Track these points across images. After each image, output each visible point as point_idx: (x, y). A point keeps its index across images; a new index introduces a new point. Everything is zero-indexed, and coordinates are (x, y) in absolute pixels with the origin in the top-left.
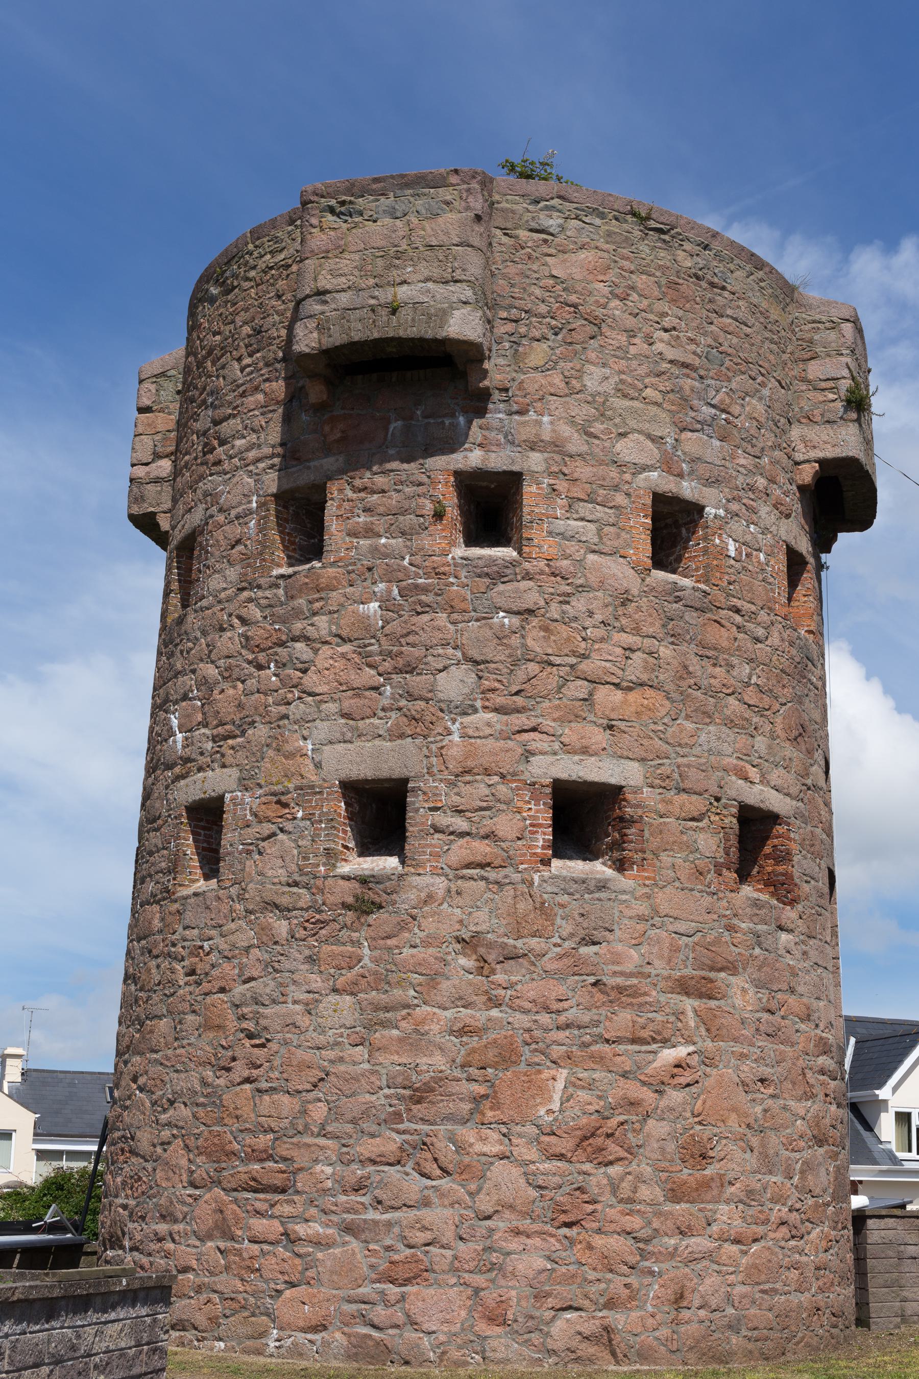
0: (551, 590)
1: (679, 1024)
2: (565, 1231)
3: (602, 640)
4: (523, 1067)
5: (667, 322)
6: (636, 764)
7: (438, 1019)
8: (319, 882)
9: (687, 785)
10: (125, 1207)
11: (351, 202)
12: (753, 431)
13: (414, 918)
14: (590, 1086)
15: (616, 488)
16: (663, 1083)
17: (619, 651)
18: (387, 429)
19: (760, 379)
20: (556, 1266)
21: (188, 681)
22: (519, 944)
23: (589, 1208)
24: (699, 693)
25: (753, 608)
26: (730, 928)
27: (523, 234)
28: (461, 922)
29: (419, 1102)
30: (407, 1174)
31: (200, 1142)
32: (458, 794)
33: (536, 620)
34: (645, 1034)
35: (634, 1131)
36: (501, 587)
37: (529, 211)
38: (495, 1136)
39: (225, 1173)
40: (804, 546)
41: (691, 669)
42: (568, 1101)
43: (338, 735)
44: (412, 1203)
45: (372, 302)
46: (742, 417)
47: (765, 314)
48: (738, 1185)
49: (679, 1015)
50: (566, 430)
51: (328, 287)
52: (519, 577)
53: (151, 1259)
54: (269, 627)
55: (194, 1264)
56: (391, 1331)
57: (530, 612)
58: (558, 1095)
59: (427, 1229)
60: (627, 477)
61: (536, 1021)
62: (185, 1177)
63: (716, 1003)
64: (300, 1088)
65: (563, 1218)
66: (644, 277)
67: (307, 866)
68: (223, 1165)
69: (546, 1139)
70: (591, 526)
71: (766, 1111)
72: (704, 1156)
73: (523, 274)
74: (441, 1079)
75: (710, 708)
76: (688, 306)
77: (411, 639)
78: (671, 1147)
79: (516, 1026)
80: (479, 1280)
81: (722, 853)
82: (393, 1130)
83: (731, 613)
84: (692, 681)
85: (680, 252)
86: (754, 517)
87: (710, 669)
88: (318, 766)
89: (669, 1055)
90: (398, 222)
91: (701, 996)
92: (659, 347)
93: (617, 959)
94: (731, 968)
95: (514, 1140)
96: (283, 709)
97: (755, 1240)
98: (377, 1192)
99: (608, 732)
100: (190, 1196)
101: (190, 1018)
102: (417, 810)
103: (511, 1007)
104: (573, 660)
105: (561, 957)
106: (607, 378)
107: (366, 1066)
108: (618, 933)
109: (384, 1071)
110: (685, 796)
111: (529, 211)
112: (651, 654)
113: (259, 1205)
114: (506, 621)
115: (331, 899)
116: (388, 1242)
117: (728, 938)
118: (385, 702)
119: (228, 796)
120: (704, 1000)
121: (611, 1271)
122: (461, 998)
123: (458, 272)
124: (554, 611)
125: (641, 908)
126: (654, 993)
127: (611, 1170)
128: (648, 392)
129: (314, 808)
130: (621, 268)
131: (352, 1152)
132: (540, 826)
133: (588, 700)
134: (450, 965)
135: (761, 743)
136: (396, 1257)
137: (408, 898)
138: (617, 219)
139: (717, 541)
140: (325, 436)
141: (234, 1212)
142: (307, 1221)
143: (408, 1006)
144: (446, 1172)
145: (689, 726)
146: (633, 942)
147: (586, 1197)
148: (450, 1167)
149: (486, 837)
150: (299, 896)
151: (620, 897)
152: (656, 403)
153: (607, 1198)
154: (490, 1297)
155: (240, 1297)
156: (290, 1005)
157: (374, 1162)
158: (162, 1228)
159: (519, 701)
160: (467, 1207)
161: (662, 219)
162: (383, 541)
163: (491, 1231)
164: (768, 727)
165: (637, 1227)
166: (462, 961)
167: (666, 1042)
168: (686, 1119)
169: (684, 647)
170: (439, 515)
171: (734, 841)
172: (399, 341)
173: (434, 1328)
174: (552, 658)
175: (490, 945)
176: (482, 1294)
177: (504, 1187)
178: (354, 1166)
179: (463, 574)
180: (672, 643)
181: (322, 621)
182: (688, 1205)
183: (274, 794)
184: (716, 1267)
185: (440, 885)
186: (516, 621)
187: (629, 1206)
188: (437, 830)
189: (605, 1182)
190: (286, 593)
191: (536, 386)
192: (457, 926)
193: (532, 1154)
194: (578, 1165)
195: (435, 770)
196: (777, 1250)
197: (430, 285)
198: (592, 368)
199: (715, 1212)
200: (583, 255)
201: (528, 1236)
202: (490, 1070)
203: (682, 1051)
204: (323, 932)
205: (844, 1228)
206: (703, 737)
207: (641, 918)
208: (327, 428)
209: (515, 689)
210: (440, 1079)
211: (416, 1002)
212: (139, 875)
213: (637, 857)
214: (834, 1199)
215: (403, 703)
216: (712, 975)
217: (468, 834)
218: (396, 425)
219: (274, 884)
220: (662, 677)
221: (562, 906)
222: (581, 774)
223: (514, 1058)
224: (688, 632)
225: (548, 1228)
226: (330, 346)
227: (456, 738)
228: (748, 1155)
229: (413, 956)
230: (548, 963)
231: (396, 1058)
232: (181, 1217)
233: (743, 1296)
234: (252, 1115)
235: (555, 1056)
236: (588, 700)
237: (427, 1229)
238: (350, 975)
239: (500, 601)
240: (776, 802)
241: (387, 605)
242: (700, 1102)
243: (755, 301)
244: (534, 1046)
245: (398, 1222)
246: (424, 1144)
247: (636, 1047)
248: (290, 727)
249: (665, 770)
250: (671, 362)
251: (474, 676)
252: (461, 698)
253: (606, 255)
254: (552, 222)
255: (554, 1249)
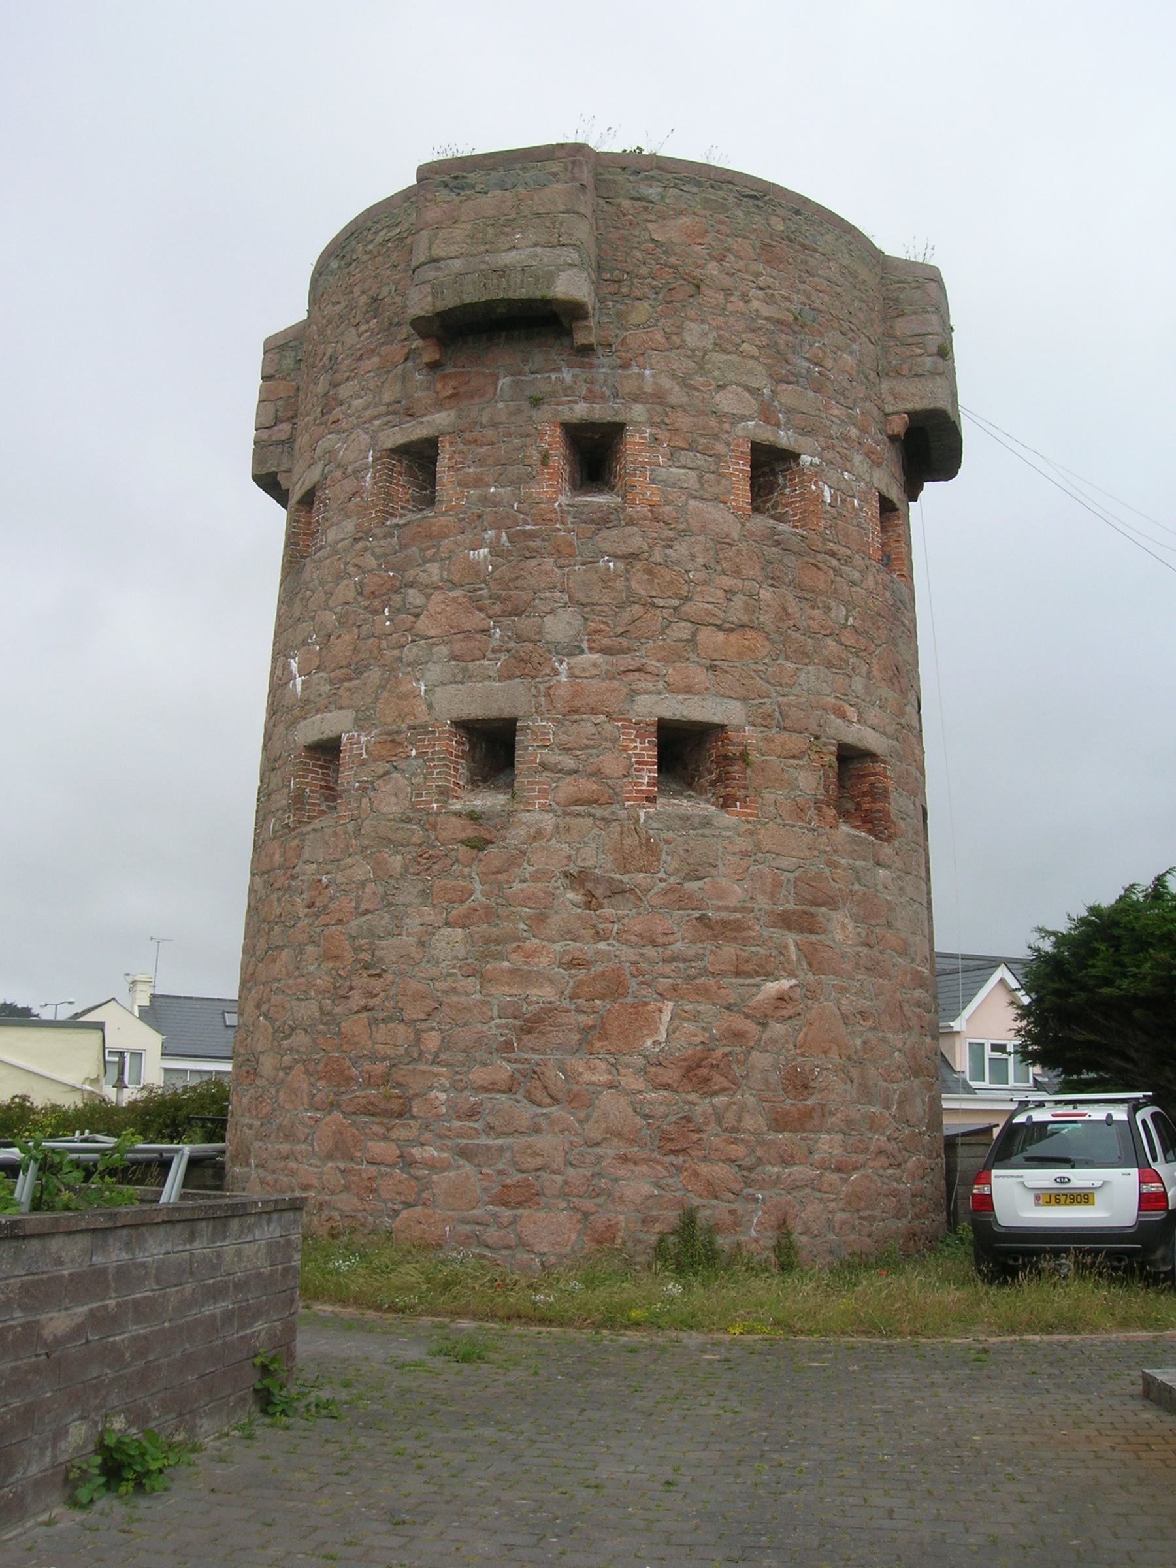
0: (655, 535)
1: (782, 958)
2: (671, 1158)
3: (705, 583)
4: (629, 1000)
5: (762, 281)
6: (738, 704)
7: (547, 954)
8: (431, 819)
9: (788, 723)
10: (250, 1127)
11: (464, 177)
12: (845, 384)
13: (524, 853)
14: (696, 1017)
15: (716, 437)
16: (766, 1016)
17: (720, 593)
18: (496, 386)
19: (851, 335)
20: (663, 1192)
21: (307, 626)
22: (625, 878)
23: (695, 1137)
24: (797, 635)
25: (849, 552)
26: (832, 864)
27: (626, 204)
28: (569, 857)
29: (529, 1032)
30: (518, 1102)
31: (320, 1067)
32: (565, 733)
33: (641, 564)
34: (748, 967)
35: (738, 1062)
36: (605, 533)
37: (629, 181)
38: (604, 1066)
39: (344, 1097)
40: (895, 494)
41: (790, 610)
42: (674, 1032)
43: (449, 676)
44: (523, 1129)
45: (483, 267)
46: (834, 371)
47: (854, 275)
48: (839, 1115)
49: (782, 949)
50: (666, 383)
51: (442, 254)
52: (623, 523)
53: (275, 1176)
54: (383, 573)
55: (315, 1182)
56: (504, 1252)
57: (634, 556)
58: (667, 1028)
59: (538, 1155)
60: (726, 426)
61: (642, 954)
62: (306, 1100)
63: (817, 937)
64: (415, 1017)
65: (670, 1146)
66: (739, 240)
67: (419, 803)
68: (343, 1089)
69: (653, 1069)
70: (693, 474)
71: (864, 1043)
72: (805, 1086)
73: (623, 238)
74: (551, 1010)
75: (809, 649)
76: (781, 266)
77: (519, 583)
78: (774, 1078)
79: (623, 959)
80: (588, 1204)
81: (822, 791)
82: (504, 1059)
83: (828, 557)
84: (791, 623)
85: (773, 218)
86: (848, 464)
87: (809, 611)
88: (430, 706)
89: (772, 988)
90: (507, 193)
91: (802, 930)
92: (755, 304)
93: (721, 894)
94: (831, 903)
95: (622, 1071)
96: (396, 652)
97: (855, 1168)
98: (490, 1119)
99: (710, 672)
100: (310, 1117)
101: (310, 948)
102: (526, 748)
103: (618, 941)
104: (676, 603)
105: (666, 892)
106: (706, 334)
107: (477, 996)
108: (722, 869)
109: (496, 1002)
110: (786, 734)
111: (629, 181)
112: (751, 596)
113: (376, 1128)
114: (611, 564)
115: (443, 835)
116: (500, 1166)
117: (828, 874)
118: (495, 643)
119: (344, 737)
120: (806, 935)
121: (716, 1198)
122: (569, 932)
123: (564, 237)
124: (657, 556)
125: (744, 844)
126: (757, 928)
127: (715, 1100)
128: (745, 346)
129: (427, 747)
130: (718, 231)
131: (465, 1079)
132: (646, 763)
133: (692, 641)
134: (558, 898)
135: (858, 684)
136: (508, 1181)
137: (516, 836)
138: (712, 187)
139: (814, 487)
140: (437, 393)
141: (353, 1135)
142: (423, 1145)
143: (518, 939)
144: (555, 1100)
145: (790, 666)
146: (737, 877)
147: (691, 1126)
148: (560, 1096)
149: (592, 774)
150: (413, 831)
151: (723, 833)
152: (753, 357)
153: (713, 1127)
154: (599, 1221)
155: (360, 1215)
156: (404, 937)
157: (486, 1090)
158: (285, 1147)
159: (624, 642)
160: (577, 1134)
161: (755, 187)
162: (492, 490)
163: (600, 1158)
164: (865, 668)
165: (741, 1155)
166: (570, 895)
167: (770, 976)
168: (788, 1050)
169: (783, 590)
170: (545, 460)
171: (833, 778)
172: (510, 302)
173: (546, 1250)
174: (655, 600)
175: (598, 880)
176: (591, 1218)
177: (612, 1116)
178: (466, 1093)
179: (570, 519)
180: (772, 586)
181: (434, 568)
182: (790, 1135)
183: (389, 733)
184: (817, 1194)
185: (548, 821)
186: (621, 565)
187: (734, 1135)
188: (544, 766)
189: (710, 1111)
190: (400, 542)
191: (638, 343)
192: (565, 862)
193: (638, 1084)
194: (684, 1095)
195: (543, 709)
196: (876, 1178)
197: (539, 249)
198: (692, 325)
199: (817, 1142)
200: (683, 220)
201: (635, 1163)
202: (598, 1002)
203: (785, 984)
204: (436, 867)
205: (938, 1156)
206: (802, 678)
207: (745, 854)
208: (439, 386)
209: (619, 630)
210: (549, 1011)
211: (525, 934)
212: (261, 813)
213: (740, 793)
214: (928, 1128)
215: (512, 644)
216: (813, 909)
217: (576, 772)
218: (504, 381)
219: (389, 820)
220: (762, 619)
221: (667, 842)
222: (685, 713)
223: (620, 991)
224: (786, 574)
225: (656, 1155)
226: (442, 309)
227: (564, 679)
228: (848, 1086)
229: (522, 890)
230: (653, 898)
231: (507, 989)
232: (303, 1138)
233: (843, 1223)
234: (370, 1043)
235: (661, 989)
236: (692, 641)
237: (538, 1155)
238: (462, 909)
239: (606, 546)
240: (871, 740)
241: (496, 551)
242: (802, 1034)
243: (845, 262)
244: (641, 978)
245: (510, 1147)
246: (535, 1072)
247: (741, 981)
248: (403, 669)
249: (767, 709)
250: (766, 319)
251: (580, 618)
252: (567, 640)
253: (704, 220)
254: (653, 192)
255: (660, 1175)
